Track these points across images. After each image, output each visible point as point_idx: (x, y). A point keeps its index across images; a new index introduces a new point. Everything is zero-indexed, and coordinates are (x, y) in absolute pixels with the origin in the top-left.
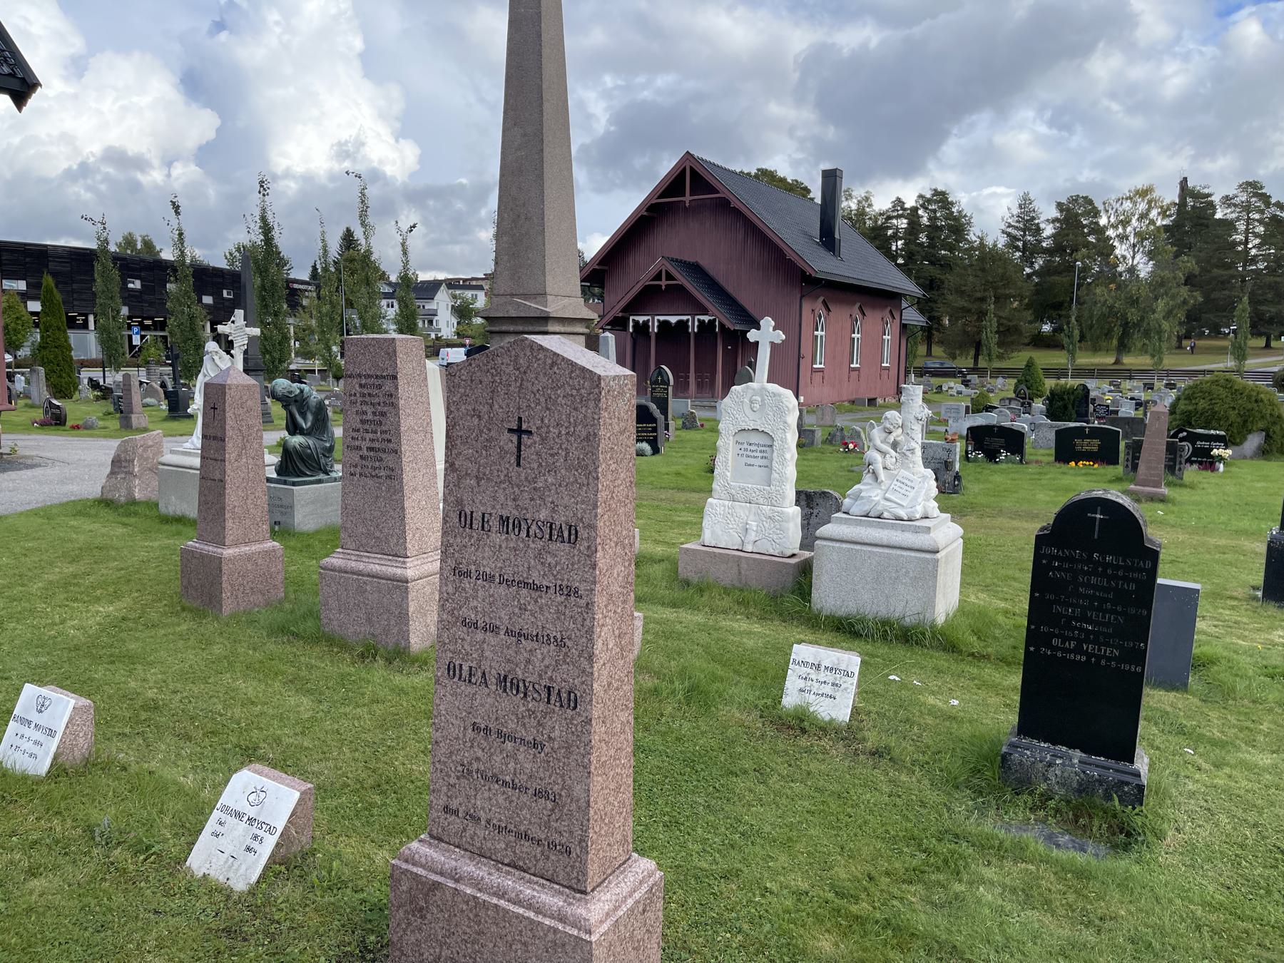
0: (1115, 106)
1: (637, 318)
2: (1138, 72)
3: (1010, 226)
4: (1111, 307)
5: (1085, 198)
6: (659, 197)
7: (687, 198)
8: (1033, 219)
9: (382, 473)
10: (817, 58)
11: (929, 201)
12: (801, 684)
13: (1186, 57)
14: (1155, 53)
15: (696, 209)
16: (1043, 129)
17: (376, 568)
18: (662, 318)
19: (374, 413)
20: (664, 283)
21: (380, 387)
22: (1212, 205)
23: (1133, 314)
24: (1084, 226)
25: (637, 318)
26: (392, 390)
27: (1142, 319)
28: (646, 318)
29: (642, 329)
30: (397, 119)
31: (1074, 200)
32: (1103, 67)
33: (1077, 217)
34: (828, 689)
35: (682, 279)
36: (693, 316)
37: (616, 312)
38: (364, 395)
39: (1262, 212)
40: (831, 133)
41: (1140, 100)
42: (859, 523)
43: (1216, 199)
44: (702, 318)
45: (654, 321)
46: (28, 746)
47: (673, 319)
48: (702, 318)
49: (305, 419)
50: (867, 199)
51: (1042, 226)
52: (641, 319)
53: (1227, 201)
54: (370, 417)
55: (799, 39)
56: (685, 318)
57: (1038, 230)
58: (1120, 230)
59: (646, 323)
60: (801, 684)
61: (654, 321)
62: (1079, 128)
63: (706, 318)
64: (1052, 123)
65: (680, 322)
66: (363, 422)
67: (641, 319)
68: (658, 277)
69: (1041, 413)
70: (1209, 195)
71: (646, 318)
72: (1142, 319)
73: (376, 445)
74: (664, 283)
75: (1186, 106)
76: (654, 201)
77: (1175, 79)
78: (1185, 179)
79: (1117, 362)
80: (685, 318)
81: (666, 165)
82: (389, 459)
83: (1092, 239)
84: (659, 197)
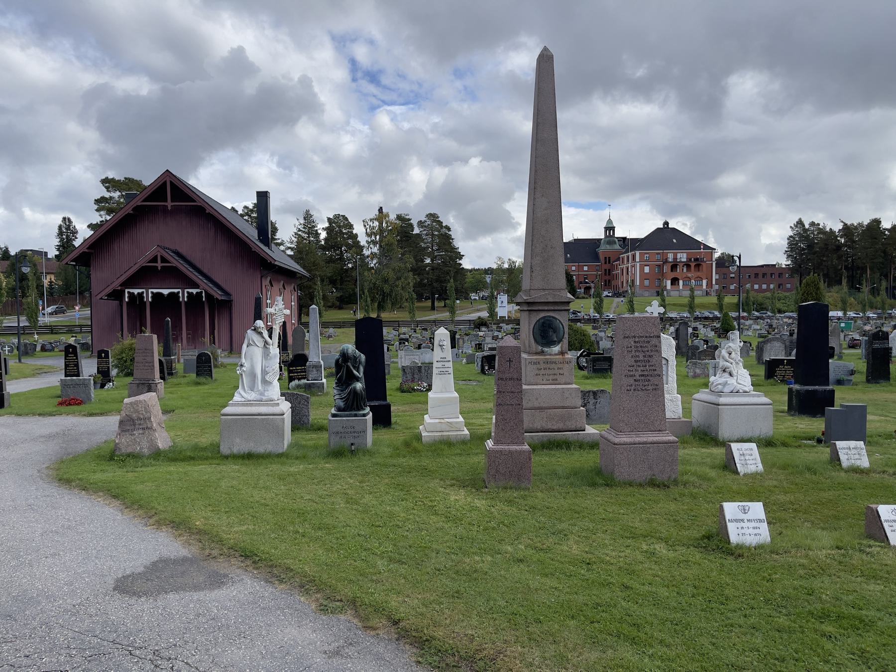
0: (316, 158)
1: (131, 291)
2: (327, 139)
3: (300, 230)
4: (375, 284)
5: (343, 216)
8: (314, 227)
9: (650, 388)
10: (95, 94)
11: (252, 211)
12: (846, 457)
13: (353, 134)
14: (333, 129)
15: (176, 211)
16: (274, 167)
17: (651, 439)
18: (155, 291)
19: (644, 356)
20: (159, 265)
21: (648, 342)
22: (411, 226)
23: (387, 289)
24: (344, 234)
25: (131, 291)
26: (657, 344)
27: (391, 291)
28: (140, 291)
29: (137, 302)
31: (337, 216)
32: (305, 130)
33: (339, 227)
34: (857, 456)
35: (176, 262)
37: (116, 285)
38: (637, 347)
39: (439, 231)
40: (111, 150)
41: (331, 157)
42: (728, 396)
43: (414, 222)
44: (190, 291)
45: (149, 294)
46: (751, 531)
47: (166, 292)
48: (190, 291)
49: (358, 371)
51: (319, 232)
52: (136, 291)
53: (420, 224)
54: (641, 358)
55: (87, 79)
57: (317, 235)
58: (373, 238)
59: (141, 295)
60: (846, 457)
61: (149, 294)
62: (296, 169)
63: (194, 291)
64: (279, 164)
65: (170, 294)
66: (636, 361)
67: (136, 291)
68: (154, 260)
70: (410, 220)
71: (140, 291)
72: (391, 291)
73: (646, 373)
74: (159, 265)
75: (356, 163)
77: (349, 146)
78: (381, 208)
79: (378, 316)
80: (176, 291)
82: (654, 380)
83: (350, 241)
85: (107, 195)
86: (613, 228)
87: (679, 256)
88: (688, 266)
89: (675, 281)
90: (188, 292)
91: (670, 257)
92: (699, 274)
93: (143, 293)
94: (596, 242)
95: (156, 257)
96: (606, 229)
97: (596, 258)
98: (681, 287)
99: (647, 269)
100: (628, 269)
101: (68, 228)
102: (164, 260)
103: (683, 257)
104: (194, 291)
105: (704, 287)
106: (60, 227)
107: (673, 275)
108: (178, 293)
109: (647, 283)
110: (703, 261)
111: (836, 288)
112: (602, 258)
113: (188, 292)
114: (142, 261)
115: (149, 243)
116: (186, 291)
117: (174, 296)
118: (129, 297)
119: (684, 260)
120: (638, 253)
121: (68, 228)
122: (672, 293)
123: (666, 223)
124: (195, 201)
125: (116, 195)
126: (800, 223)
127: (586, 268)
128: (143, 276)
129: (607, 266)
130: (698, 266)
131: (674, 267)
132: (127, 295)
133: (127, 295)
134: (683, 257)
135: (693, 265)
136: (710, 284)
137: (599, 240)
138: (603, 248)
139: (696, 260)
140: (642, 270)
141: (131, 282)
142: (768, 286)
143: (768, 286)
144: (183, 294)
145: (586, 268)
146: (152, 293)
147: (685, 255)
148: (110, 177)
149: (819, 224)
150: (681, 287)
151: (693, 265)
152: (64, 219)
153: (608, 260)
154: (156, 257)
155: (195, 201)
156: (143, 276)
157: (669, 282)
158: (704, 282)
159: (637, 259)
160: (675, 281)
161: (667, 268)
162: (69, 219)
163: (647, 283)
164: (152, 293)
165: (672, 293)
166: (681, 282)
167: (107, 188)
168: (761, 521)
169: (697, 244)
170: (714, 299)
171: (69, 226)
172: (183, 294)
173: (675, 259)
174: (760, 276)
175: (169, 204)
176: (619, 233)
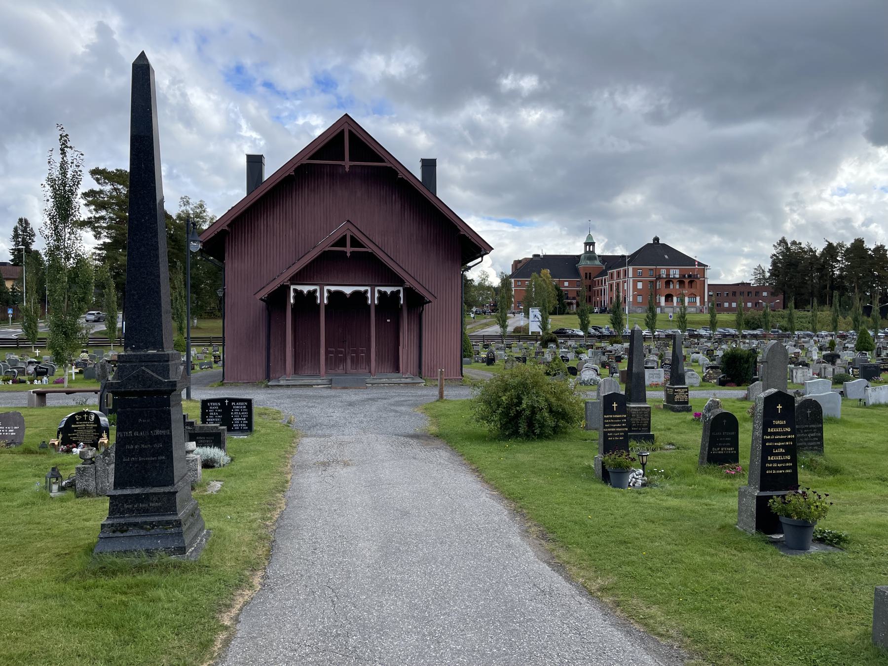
1: (299, 288)
6: (311, 158)
7: (347, 163)
18: (333, 288)
20: (349, 250)
25: (299, 288)
28: (312, 288)
29: (307, 302)
30: (87, 46)
36: (373, 287)
44: (383, 289)
47: (348, 290)
48: (383, 289)
50: (201, 206)
52: (305, 289)
56: (362, 289)
59: (312, 294)
61: (323, 293)
67: (305, 289)
68: (341, 242)
69: (657, 117)
71: (312, 288)
74: (349, 250)
76: (305, 161)
80: (362, 289)
81: (317, 125)
84: (311, 158)
85: (97, 187)
86: (593, 244)
87: (671, 272)
88: (681, 282)
89: (669, 297)
90: (379, 292)
91: (663, 273)
92: (693, 291)
93: (315, 291)
94: (576, 259)
95: (345, 237)
96: (586, 244)
97: (576, 273)
98: (675, 304)
99: (640, 285)
100: (618, 284)
101: (25, 230)
102: (355, 243)
103: (675, 273)
104: (389, 290)
105: (698, 304)
106: (16, 229)
107: (667, 292)
108: (366, 292)
109: (640, 299)
110: (697, 278)
111: (826, 307)
112: (582, 273)
113: (379, 292)
114: (324, 244)
115: (324, 220)
116: (377, 289)
117: (359, 297)
118: (295, 298)
119: (677, 276)
120: (631, 269)
121: (25, 230)
122: (666, 310)
123: (656, 239)
124: (383, 161)
125: (108, 188)
126: (783, 241)
127: (566, 284)
128: (325, 265)
129: (588, 282)
130: (691, 282)
131: (668, 283)
132: (292, 294)
133: (292, 294)
134: (675, 273)
135: (687, 281)
136: (702, 302)
137: (579, 257)
138: (583, 264)
139: (690, 276)
140: (635, 285)
141: (299, 278)
142: (730, 304)
143: (730, 304)
144: (373, 294)
145: (566, 284)
146: (329, 291)
147: (678, 272)
148: (101, 168)
149: (800, 244)
150: (675, 304)
151: (687, 281)
152: (21, 220)
153: (588, 276)
154: (345, 237)
155: (382, 161)
156: (325, 265)
157: (663, 299)
158: (698, 299)
159: (631, 275)
160: (669, 297)
161: (660, 285)
162: (26, 221)
163: (640, 299)
164: (329, 291)
165: (666, 310)
166: (675, 299)
167: (97, 180)
168: (26, 416)
169: (690, 261)
170: (707, 317)
171: (26, 228)
172: (373, 294)
173: (668, 275)
174: (738, 294)
175: (347, 163)
176: (598, 251)
